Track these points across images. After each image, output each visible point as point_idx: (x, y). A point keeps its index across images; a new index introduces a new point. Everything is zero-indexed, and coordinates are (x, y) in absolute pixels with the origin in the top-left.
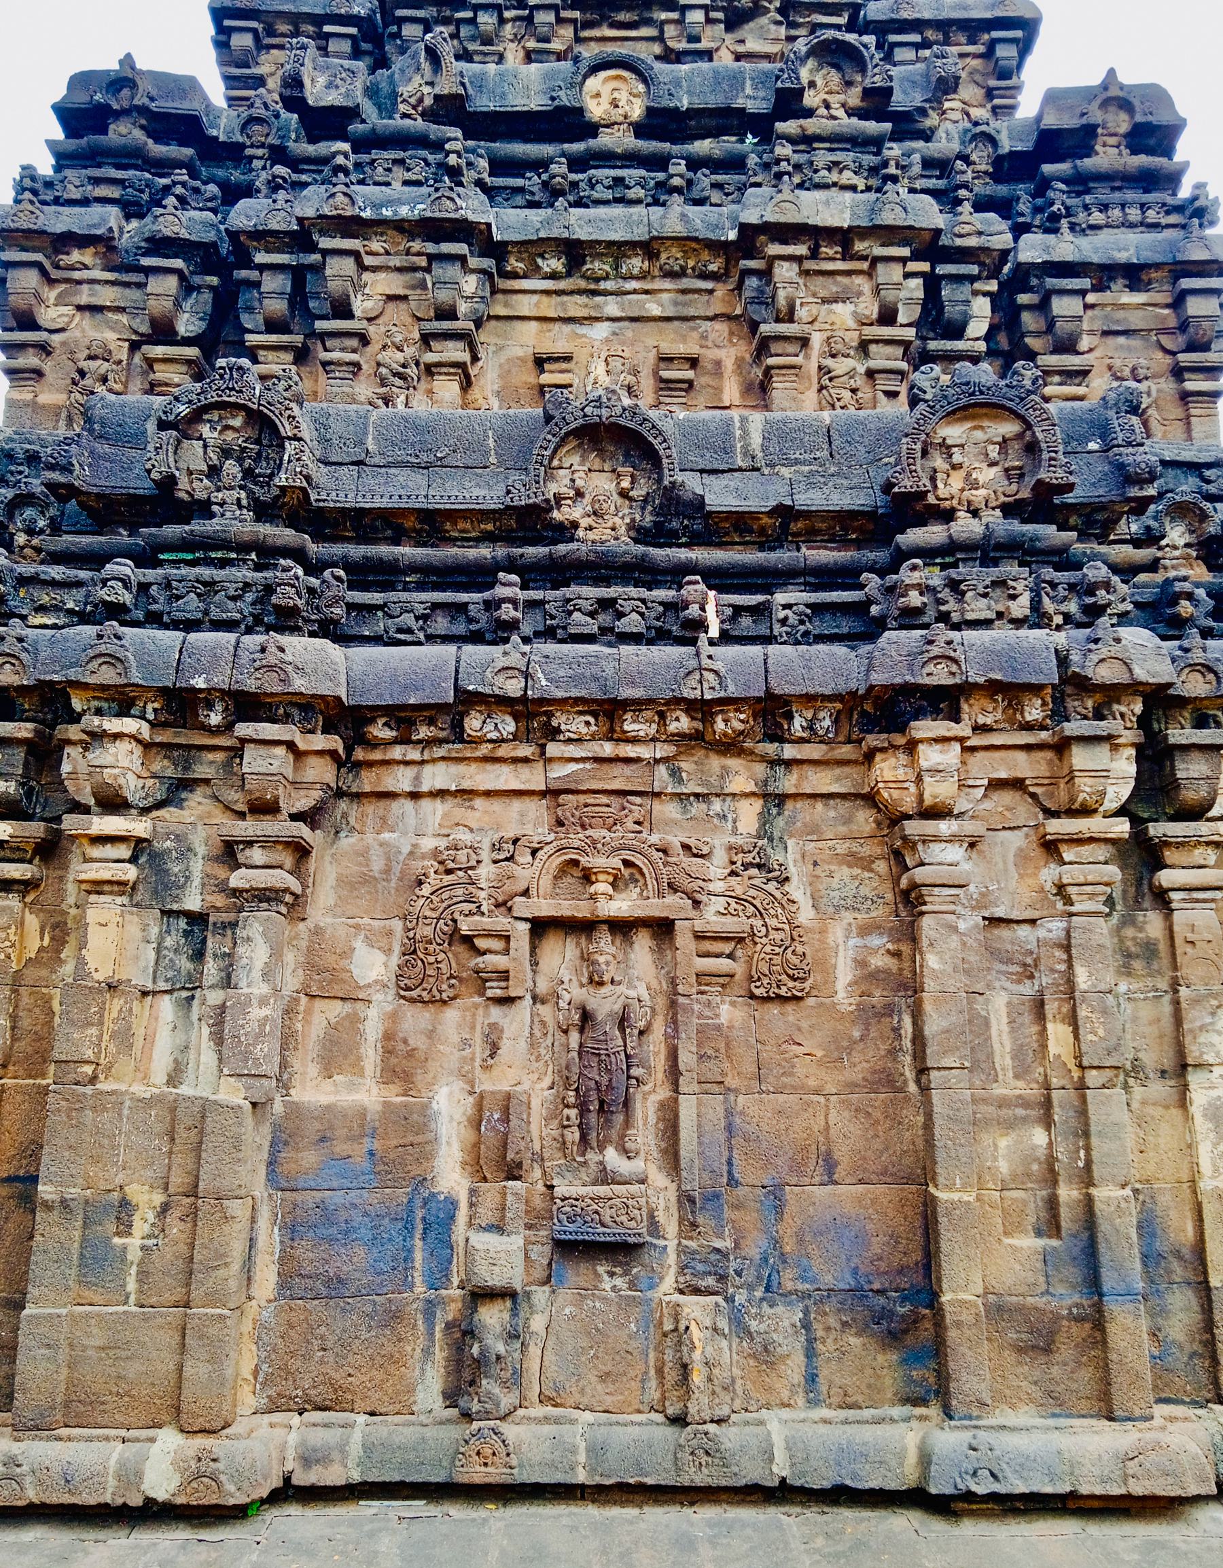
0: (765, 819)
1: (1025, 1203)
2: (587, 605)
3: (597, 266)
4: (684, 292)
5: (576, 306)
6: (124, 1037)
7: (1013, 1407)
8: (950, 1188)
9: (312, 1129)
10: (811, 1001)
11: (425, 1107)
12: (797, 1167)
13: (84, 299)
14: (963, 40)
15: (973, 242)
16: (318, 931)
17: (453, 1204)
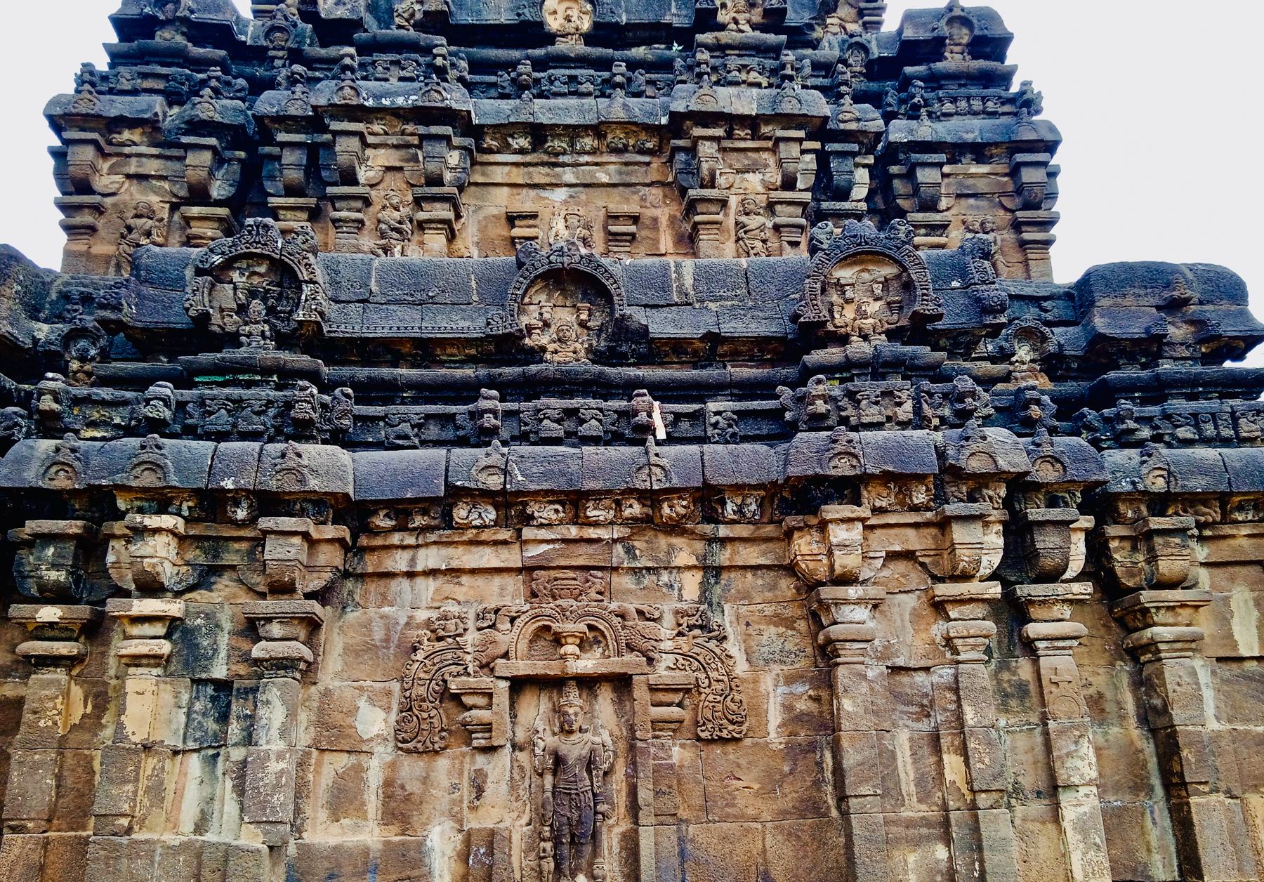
0: (705, 588)
3: (557, 144)
4: (627, 164)
5: (540, 175)
6: (156, 792)
10: (748, 742)
11: (421, 844)
15: (853, 126)
16: (327, 693)
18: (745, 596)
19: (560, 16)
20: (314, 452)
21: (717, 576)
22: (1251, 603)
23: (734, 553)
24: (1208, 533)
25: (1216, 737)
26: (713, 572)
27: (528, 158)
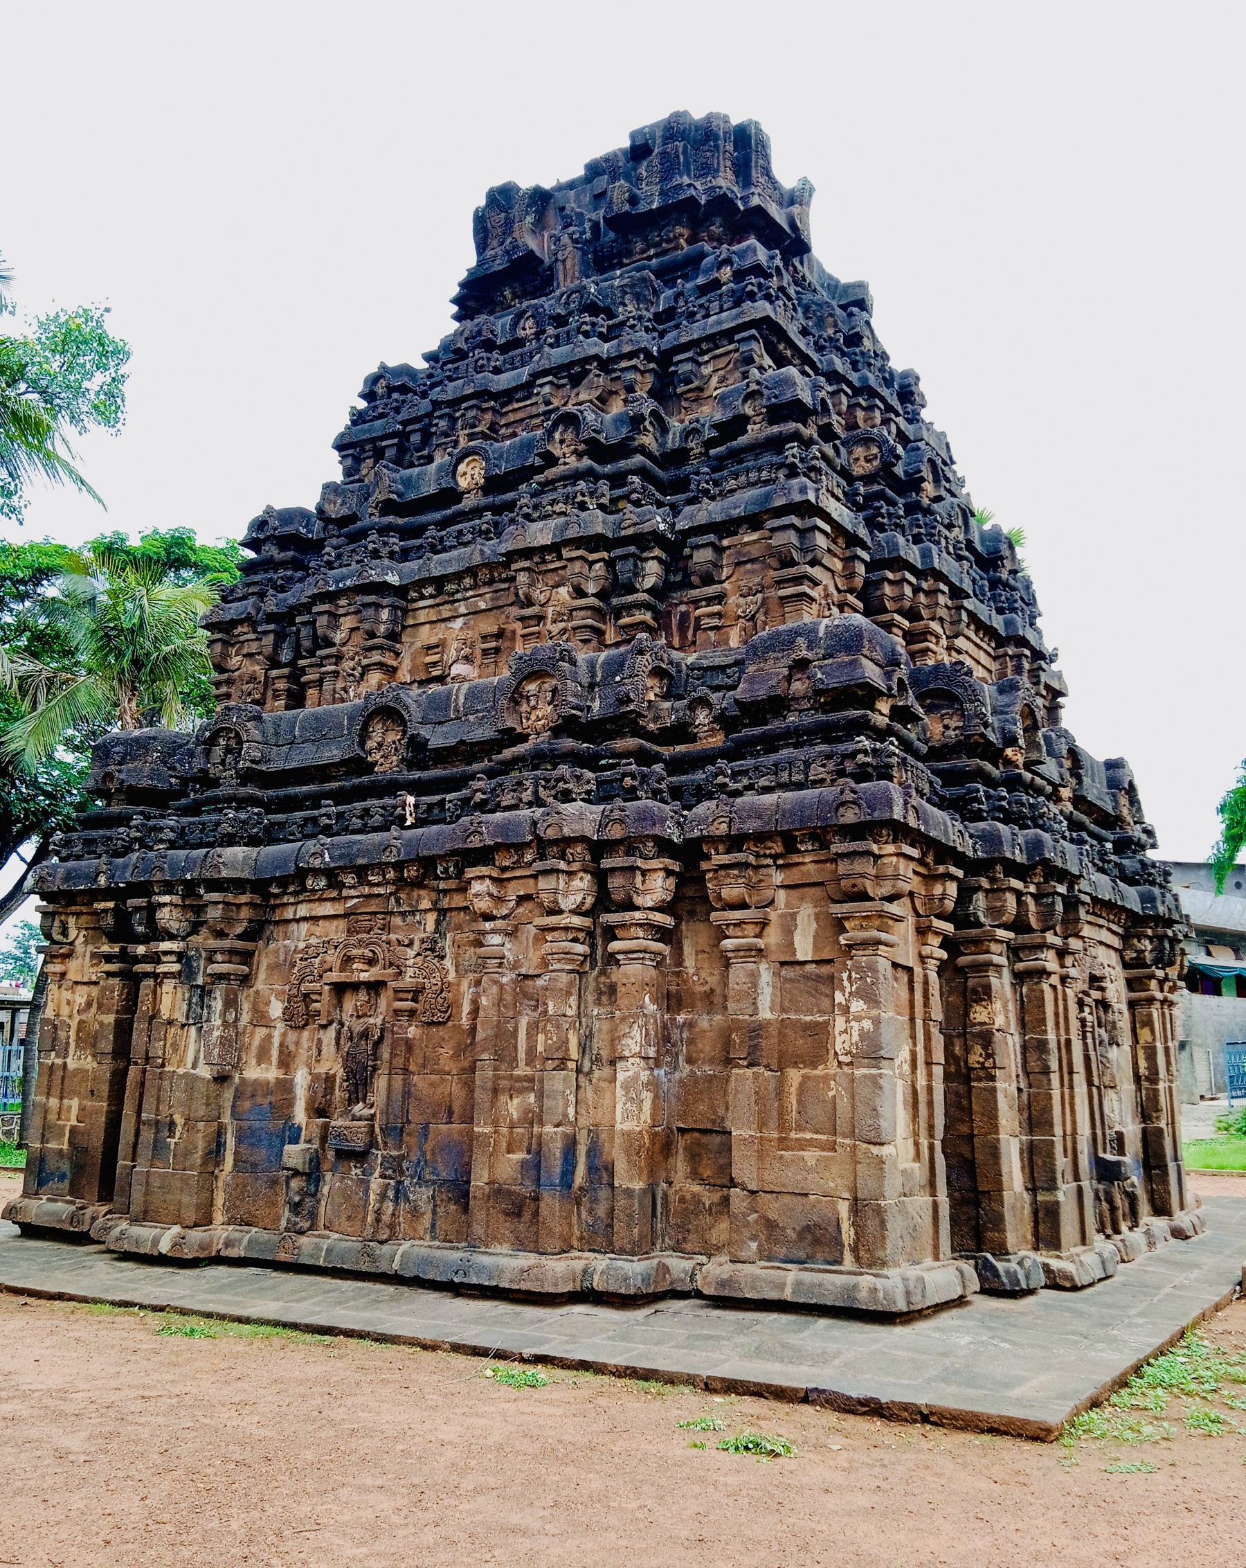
0: (438, 923)
1: (523, 1135)
2: (358, 813)
3: (449, 587)
4: (496, 591)
5: (446, 611)
6: (175, 1046)
7: (500, 1243)
8: (478, 1125)
10: (450, 1024)
11: (292, 1080)
12: (435, 1115)
13: (245, 651)
14: (725, 342)
15: (631, 531)
16: (257, 992)
17: (300, 1129)
18: (459, 927)
19: (468, 477)
20: (230, 853)
21: (444, 916)
22: (812, 918)
24: (780, 862)
25: (769, 1022)
26: (443, 912)
27: (438, 601)
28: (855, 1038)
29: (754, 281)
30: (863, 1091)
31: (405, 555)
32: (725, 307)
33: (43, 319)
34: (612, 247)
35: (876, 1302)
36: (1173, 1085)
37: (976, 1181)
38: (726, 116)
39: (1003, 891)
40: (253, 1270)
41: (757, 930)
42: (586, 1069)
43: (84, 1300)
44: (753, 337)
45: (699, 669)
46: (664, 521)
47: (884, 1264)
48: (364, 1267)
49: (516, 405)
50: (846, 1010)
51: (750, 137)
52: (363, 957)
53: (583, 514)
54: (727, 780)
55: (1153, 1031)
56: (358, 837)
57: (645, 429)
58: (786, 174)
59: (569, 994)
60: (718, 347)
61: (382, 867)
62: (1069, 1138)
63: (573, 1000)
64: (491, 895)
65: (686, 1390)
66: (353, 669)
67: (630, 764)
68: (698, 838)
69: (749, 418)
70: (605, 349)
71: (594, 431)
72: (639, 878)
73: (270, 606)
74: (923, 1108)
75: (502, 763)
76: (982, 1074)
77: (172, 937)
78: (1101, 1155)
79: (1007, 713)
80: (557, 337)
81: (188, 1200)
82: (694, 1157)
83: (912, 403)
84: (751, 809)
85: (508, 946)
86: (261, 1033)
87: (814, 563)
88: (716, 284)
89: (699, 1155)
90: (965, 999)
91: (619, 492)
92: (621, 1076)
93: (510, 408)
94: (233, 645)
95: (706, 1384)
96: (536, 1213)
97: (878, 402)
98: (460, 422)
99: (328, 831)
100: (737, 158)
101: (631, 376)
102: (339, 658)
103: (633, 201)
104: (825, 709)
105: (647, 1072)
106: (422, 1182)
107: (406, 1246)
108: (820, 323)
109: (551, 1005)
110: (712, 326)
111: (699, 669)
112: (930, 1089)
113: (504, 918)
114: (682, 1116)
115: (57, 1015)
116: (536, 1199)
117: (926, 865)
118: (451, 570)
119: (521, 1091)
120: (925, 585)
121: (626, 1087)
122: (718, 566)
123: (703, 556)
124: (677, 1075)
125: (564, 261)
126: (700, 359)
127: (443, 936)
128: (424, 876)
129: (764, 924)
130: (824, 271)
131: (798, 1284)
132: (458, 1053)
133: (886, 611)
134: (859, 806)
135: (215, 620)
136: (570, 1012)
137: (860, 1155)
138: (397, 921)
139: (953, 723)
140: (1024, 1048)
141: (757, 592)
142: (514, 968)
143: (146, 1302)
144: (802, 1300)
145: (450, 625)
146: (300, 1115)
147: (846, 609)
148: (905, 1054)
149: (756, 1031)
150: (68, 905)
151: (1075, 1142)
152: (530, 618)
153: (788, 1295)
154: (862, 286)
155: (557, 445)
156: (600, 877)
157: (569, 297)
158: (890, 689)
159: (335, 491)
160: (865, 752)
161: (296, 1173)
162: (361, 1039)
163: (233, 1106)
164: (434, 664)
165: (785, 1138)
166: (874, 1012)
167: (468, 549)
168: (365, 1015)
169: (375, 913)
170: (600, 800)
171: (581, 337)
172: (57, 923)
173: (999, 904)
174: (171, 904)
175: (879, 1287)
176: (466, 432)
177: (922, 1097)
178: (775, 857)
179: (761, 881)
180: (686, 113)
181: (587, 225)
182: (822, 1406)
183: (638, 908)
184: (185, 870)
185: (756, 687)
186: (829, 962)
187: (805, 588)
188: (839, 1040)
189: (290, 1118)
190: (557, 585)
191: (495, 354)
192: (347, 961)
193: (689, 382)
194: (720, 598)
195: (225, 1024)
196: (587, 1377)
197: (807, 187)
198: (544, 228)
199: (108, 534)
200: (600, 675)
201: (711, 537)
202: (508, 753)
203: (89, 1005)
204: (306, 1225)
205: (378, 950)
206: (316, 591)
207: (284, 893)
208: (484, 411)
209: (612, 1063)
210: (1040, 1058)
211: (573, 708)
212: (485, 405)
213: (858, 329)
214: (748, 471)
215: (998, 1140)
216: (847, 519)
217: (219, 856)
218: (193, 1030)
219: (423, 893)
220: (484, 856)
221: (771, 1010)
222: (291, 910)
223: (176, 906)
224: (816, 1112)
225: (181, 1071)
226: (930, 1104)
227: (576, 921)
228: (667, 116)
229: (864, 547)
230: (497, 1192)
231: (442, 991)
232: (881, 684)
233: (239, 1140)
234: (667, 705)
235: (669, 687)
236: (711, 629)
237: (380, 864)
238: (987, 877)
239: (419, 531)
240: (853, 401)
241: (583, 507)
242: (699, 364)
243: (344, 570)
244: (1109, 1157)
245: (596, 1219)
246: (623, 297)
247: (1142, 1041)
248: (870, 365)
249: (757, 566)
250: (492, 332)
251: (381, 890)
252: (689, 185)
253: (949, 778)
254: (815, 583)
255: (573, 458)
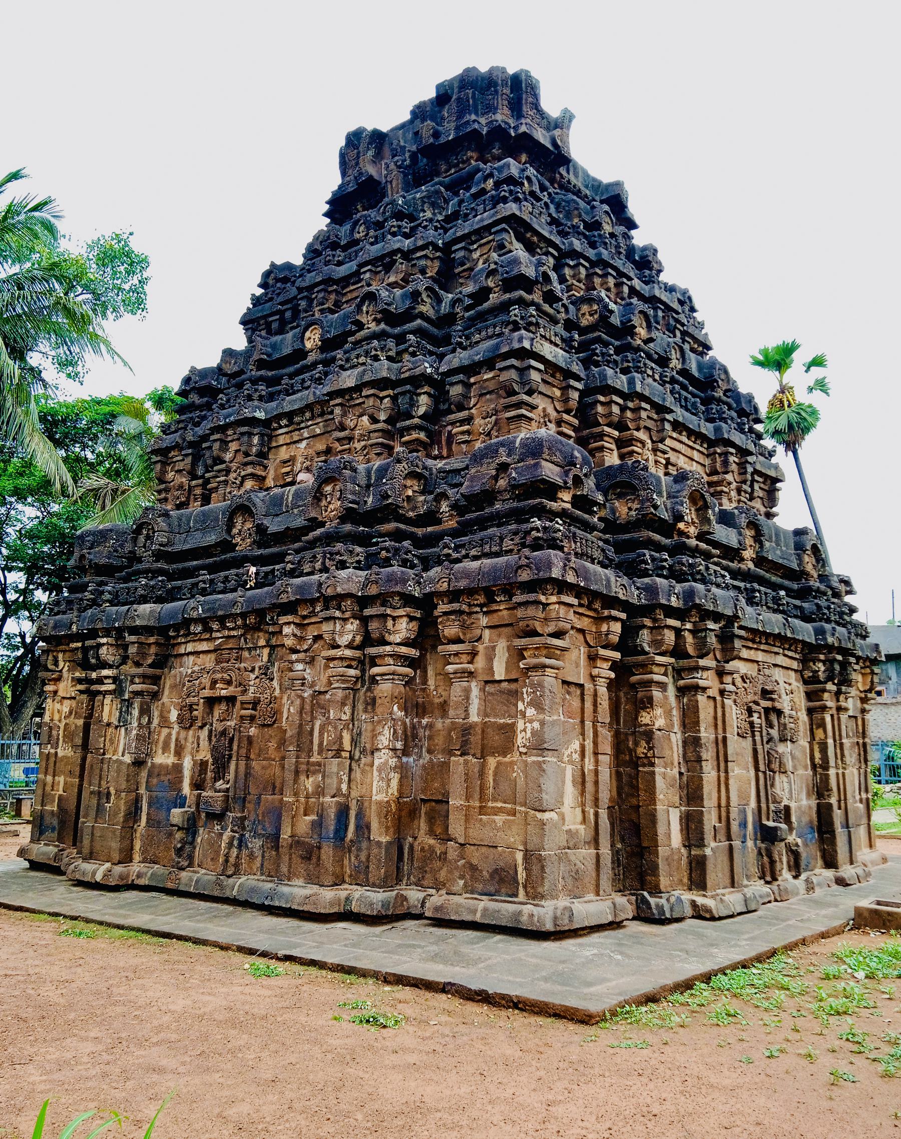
0: (270, 655)
3: (297, 419)
4: (326, 421)
8: (286, 796)
9: (156, 771)
10: (276, 725)
12: (265, 789)
13: (176, 468)
15: (407, 375)
19: (312, 340)
22: (505, 649)
23: (277, 638)
24: (485, 609)
25: (476, 724)
26: (273, 648)
27: (290, 429)
28: (529, 735)
29: (506, 188)
30: (534, 773)
31: (271, 397)
32: (487, 208)
33: (90, 243)
34: (425, 169)
35: (532, 924)
36: (846, 772)
37: (640, 839)
38: (504, 68)
39: (663, 628)
40: (154, 894)
41: (469, 658)
42: (357, 757)
43: (33, 911)
44: (504, 230)
45: (444, 472)
46: (431, 366)
47: (542, 897)
48: (216, 893)
49: (352, 288)
50: (524, 715)
51: (521, 82)
52: (223, 679)
53: (376, 364)
54: (450, 551)
55: (825, 731)
56: (220, 596)
57: (423, 301)
58: (551, 105)
59: (343, 704)
60: (482, 238)
61: (234, 617)
62: (723, 810)
63: (347, 709)
64: (295, 635)
65: (371, 981)
66: (236, 479)
67: (385, 541)
68: (429, 593)
69: (492, 289)
70: (407, 243)
71: (386, 304)
72: (390, 623)
73: (190, 437)
74: (590, 786)
75: (308, 542)
76: (645, 761)
77: (110, 667)
78: (765, 822)
79: (677, 497)
80: (376, 237)
81: (115, 845)
82: (431, 820)
83: (651, 269)
84: (463, 572)
85: (308, 671)
86: (165, 731)
87: (530, 393)
88: (483, 192)
89: (434, 818)
90: (636, 705)
91: (402, 347)
92: (377, 762)
93: (348, 290)
94: (169, 464)
95: (385, 978)
96: (319, 859)
97: (610, 271)
98: (315, 302)
99: (204, 592)
100: (513, 99)
101: (423, 262)
102: (228, 471)
103: (436, 135)
104: (519, 498)
105: (395, 760)
106: (256, 835)
107: (243, 879)
108: (568, 216)
109: (332, 711)
110: (477, 223)
111: (444, 472)
112: (596, 772)
113: (306, 651)
114: (424, 791)
115: (52, 720)
116: (319, 848)
117: (595, 610)
118: (296, 407)
119: (314, 773)
120: (630, 405)
121: (380, 770)
122: (466, 397)
123: (455, 391)
124: (421, 761)
125: (391, 182)
126: (471, 248)
127: (273, 665)
128: (260, 623)
129: (473, 654)
130: (588, 176)
131: (485, 910)
132: (278, 748)
133: (600, 425)
134: (531, 568)
135: (156, 447)
136: (344, 717)
137: (529, 819)
138: (246, 654)
139: (635, 506)
140: (685, 743)
141: (493, 415)
142: (311, 687)
143: (68, 914)
144: (486, 922)
145: (299, 445)
146: (186, 789)
147: (563, 424)
148: (576, 745)
149: (467, 730)
150: (57, 645)
151: (728, 812)
152: (343, 439)
153: (478, 918)
154: (618, 184)
155: (365, 315)
156: (365, 621)
157: (385, 207)
158: (566, 483)
159: (230, 355)
160: (538, 530)
161: (180, 829)
162: (221, 736)
163: (147, 782)
164: (287, 473)
165: (485, 807)
166: (541, 717)
167: (307, 392)
168: (224, 720)
169: (231, 649)
170: (368, 567)
171: (389, 237)
172: (50, 657)
173: (659, 638)
174: (108, 644)
175: (535, 913)
176: (318, 308)
177: (589, 778)
178: (481, 606)
179: (473, 623)
180: (474, 68)
181: (407, 155)
182: (453, 995)
183: (390, 644)
184: (115, 620)
185: (475, 484)
186: (516, 680)
187: (523, 412)
188: (520, 736)
189: (180, 790)
190: (361, 415)
191: (338, 252)
192: (214, 683)
193: (463, 264)
194: (469, 420)
195: (140, 726)
196: (313, 971)
197: (567, 115)
198: (382, 159)
199: (160, 388)
200: (373, 478)
201: (461, 377)
202: (312, 535)
203: (71, 713)
204: (186, 864)
205: (233, 674)
206: (212, 425)
207: (178, 636)
208: (330, 293)
209: (372, 753)
210: (695, 751)
211: (350, 502)
212: (330, 289)
213: (597, 218)
214: (487, 328)
215: (655, 810)
216: (561, 360)
217: (135, 611)
218: (123, 729)
219: (261, 634)
220: (289, 608)
221: (478, 715)
222: (183, 647)
223: (112, 645)
224: (504, 787)
225: (115, 758)
226: (596, 783)
227: (348, 653)
228: (461, 71)
229: (578, 378)
230: (296, 842)
231: (271, 703)
232: (559, 481)
233: (150, 806)
234: (422, 498)
235: (425, 485)
236: (464, 442)
237: (232, 614)
238: (651, 618)
239: (276, 381)
240: (591, 271)
241: (376, 358)
242: (471, 251)
243: (230, 410)
244: (771, 824)
245: (360, 862)
246: (423, 206)
247: (817, 739)
248: (606, 244)
249: (494, 396)
250: (336, 236)
251: (234, 633)
252: (474, 121)
253: (620, 547)
254: (533, 407)
255: (374, 324)
